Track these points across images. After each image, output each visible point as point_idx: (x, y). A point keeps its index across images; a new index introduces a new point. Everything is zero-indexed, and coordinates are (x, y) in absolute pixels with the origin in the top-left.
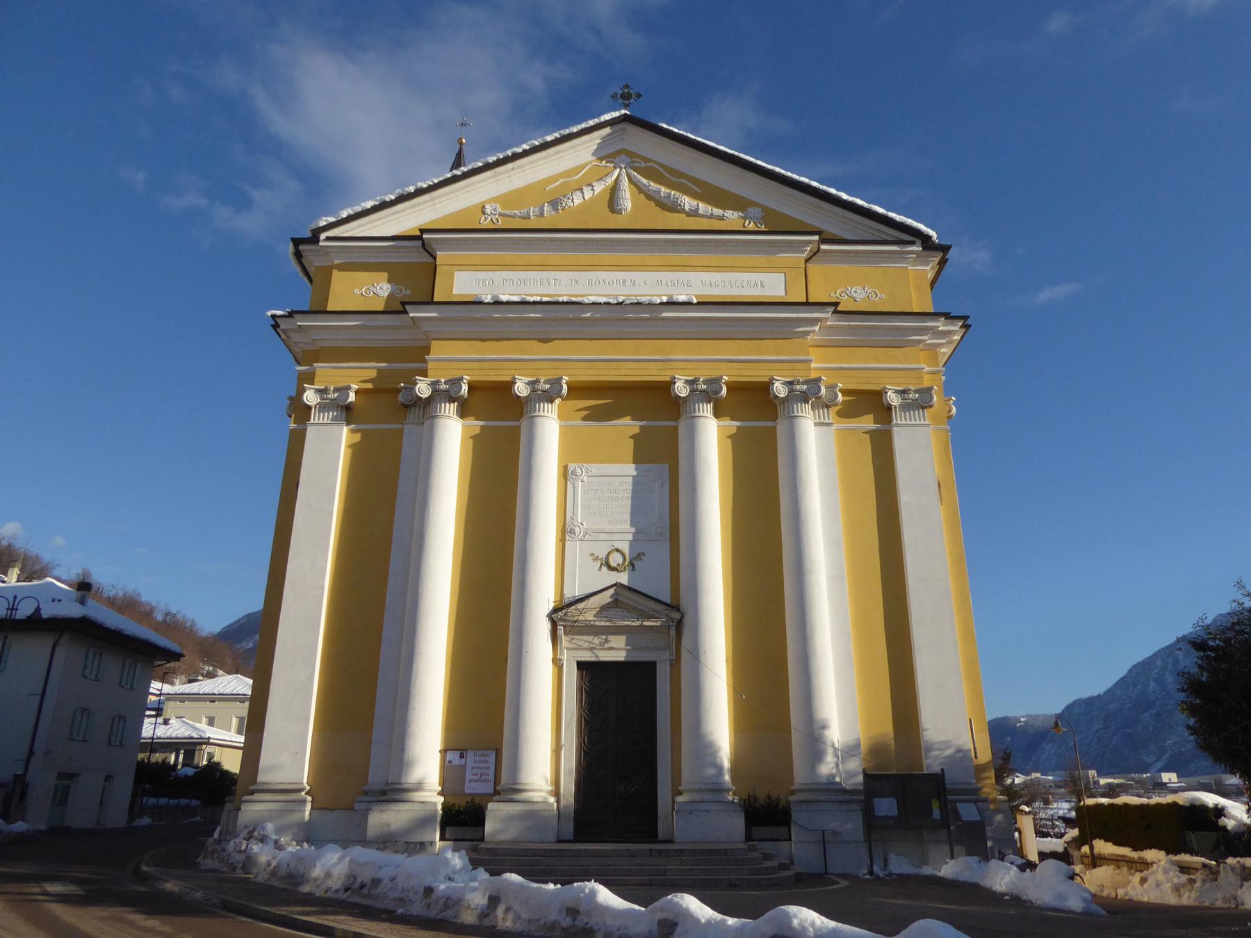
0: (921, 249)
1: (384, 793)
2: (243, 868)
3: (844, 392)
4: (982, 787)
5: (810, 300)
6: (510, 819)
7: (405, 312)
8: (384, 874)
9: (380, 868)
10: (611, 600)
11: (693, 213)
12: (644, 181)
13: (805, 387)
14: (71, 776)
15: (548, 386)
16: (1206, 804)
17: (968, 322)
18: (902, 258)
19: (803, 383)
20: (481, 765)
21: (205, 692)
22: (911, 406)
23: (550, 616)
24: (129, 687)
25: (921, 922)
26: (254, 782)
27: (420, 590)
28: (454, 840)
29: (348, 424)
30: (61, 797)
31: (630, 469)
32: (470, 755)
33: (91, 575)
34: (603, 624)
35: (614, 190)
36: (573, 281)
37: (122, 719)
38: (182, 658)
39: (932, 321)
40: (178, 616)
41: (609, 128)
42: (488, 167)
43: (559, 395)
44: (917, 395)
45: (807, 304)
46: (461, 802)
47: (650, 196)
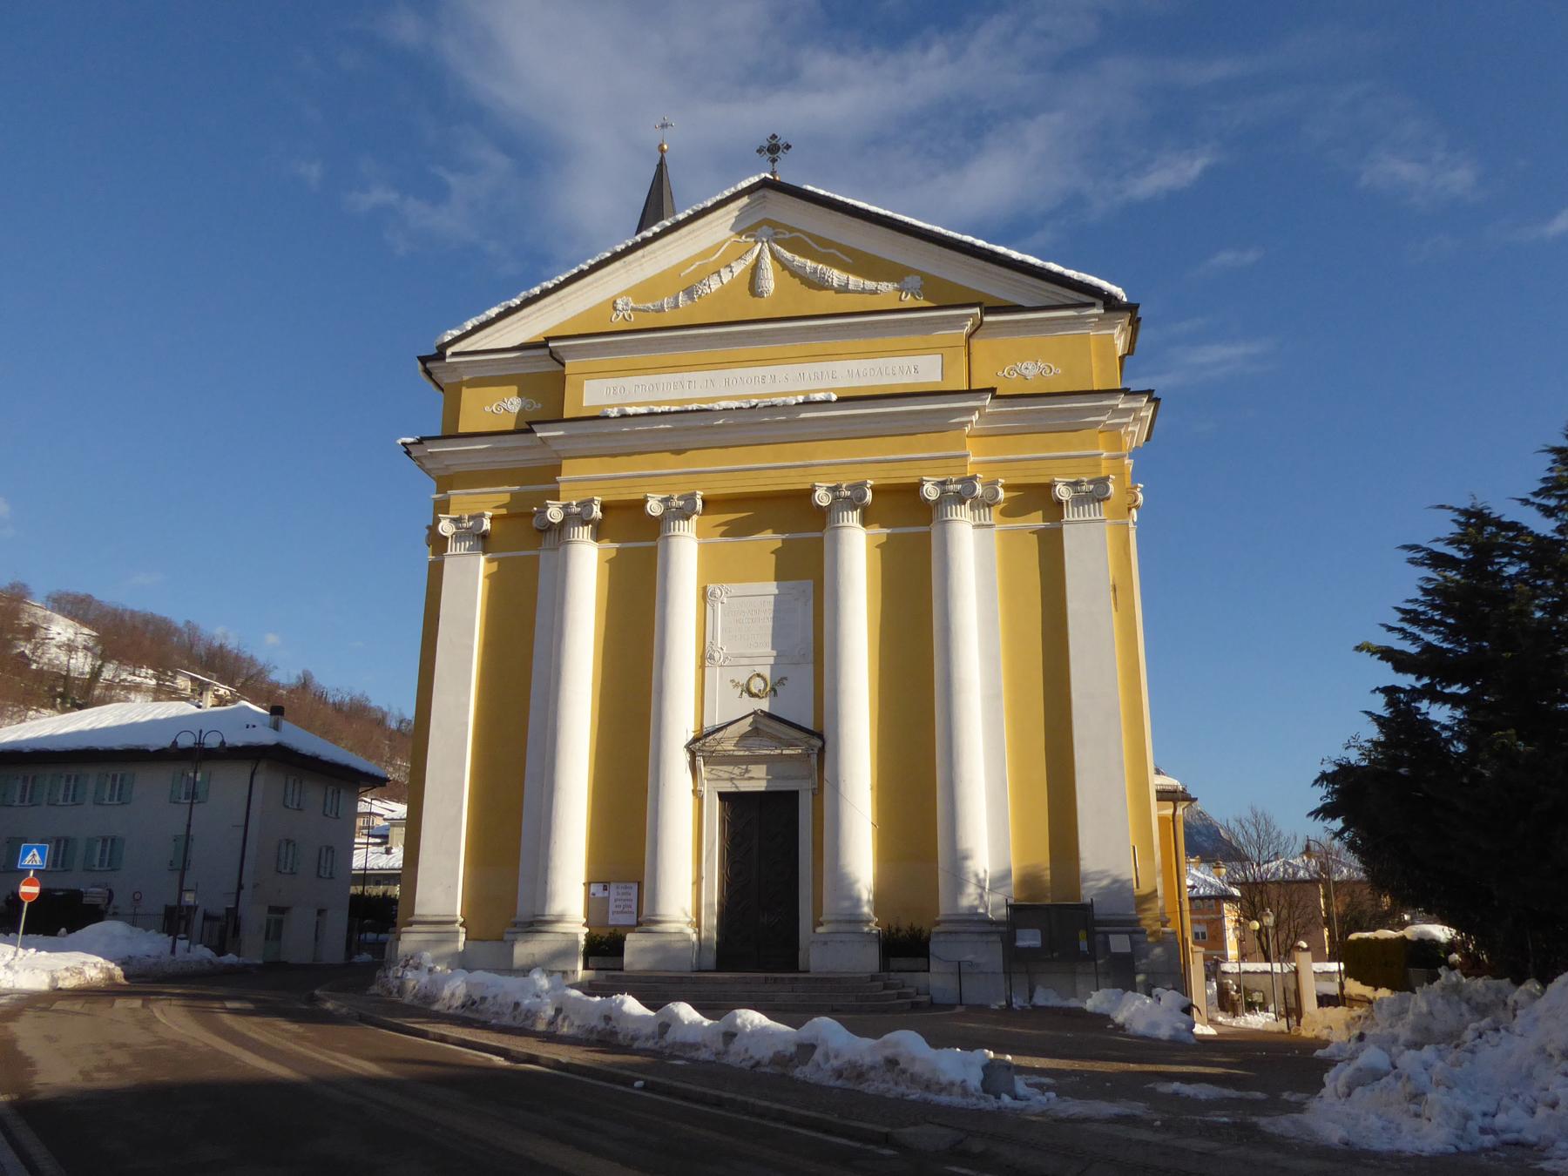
0: (1103, 311)
1: (531, 924)
2: (398, 992)
3: (1007, 488)
4: (1144, 919)
5: (973, 388)
6: (643, 950)
7: (532, 431)
8: (489, 994)
9: (488, 987)
10: (750, 728)
11: (843, 289)
12: (788, 255)
13: (959, 487)
14: (282, 910)
15: (681, 503)
16: (1437, 939)
17: (1155, 395)
18: (1082, 323)
19: (957, 482)
20: (624, 897)
22: (1085, 499)
23: (688, 747)
24: (333, 815)
26: (412, 914)
27: (558, 724)
28: (597, 969)
29: (485, 552)
30: (274, 931)
31: (772, 587)
32: (613, 887)
33: (313, 677)
34: (741, 753)
35: (756, 269)
36: (709, 382)
37: (330, 849)
38: (387, 783)
39: (1109, 399)
41: (747, 197)
42: (616, 257)
43: (693, 511)
44: (1091, 487)
45: (970, 391)
46: (605, 933)
47: (795, 273)
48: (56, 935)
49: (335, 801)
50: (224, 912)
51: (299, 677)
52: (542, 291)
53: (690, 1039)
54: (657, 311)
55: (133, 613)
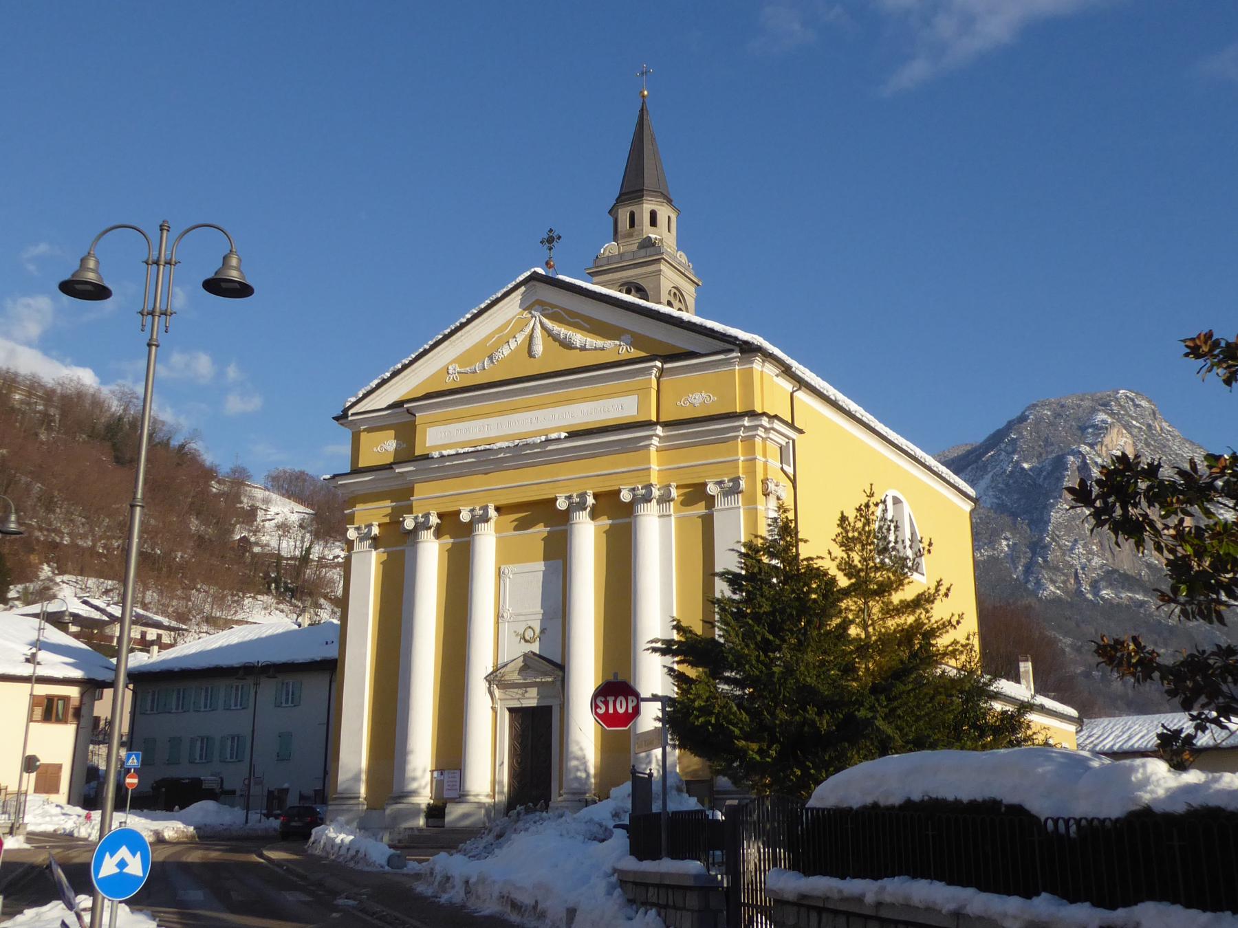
3: (678, 487)
7: (392, 468)
31: (541, 566)
39: (738, 421)
42: (446, 338)
48: (173, 811)
50: (312, 793)
54: (474, 373)
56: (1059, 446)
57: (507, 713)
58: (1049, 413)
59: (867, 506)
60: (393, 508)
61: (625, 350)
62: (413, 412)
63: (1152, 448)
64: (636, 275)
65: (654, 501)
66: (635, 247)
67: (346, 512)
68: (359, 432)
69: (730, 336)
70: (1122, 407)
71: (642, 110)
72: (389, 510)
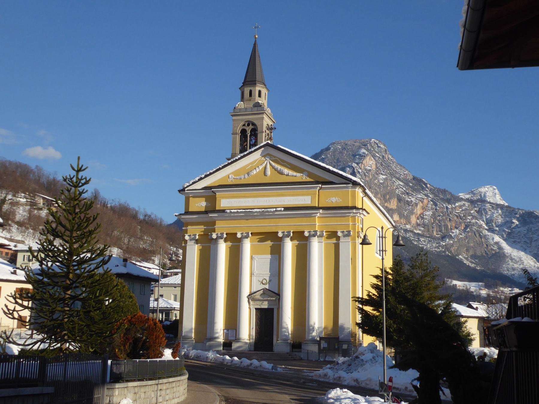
3: (326, 232)
21: (171, 283)
23: (247, 297)
25: (243, 359)
29: (197, 244)
31: (269, 256)
33: (99, 193)
35: (265, 168)
40: (152, 216)
46: (228, 342)
49: (144, 289)
51: (92, 193)
52: (210, 173)
53: (236, 363)
55: (10, 163)
56: (343, 163)
57: (255, 310)
58: (340, 147)
59: (420, 254)
60: (205, 229)
61: (305, 178)
62: (215, 192)
63: (383, 166)
64: (253, 118)
65: (316, 236)
66: (251, 106)
67: (183, 228)
68: (189, 197)
69: (349, 178)
70: (373, 147)
71: (255, 44)
72: (203, 230)
